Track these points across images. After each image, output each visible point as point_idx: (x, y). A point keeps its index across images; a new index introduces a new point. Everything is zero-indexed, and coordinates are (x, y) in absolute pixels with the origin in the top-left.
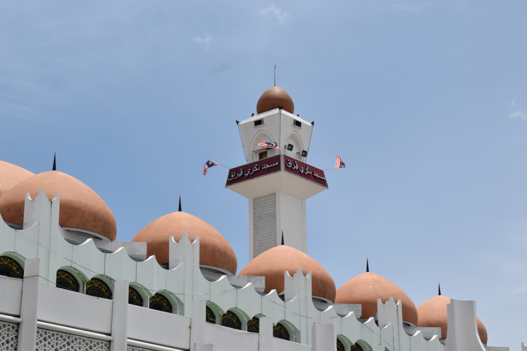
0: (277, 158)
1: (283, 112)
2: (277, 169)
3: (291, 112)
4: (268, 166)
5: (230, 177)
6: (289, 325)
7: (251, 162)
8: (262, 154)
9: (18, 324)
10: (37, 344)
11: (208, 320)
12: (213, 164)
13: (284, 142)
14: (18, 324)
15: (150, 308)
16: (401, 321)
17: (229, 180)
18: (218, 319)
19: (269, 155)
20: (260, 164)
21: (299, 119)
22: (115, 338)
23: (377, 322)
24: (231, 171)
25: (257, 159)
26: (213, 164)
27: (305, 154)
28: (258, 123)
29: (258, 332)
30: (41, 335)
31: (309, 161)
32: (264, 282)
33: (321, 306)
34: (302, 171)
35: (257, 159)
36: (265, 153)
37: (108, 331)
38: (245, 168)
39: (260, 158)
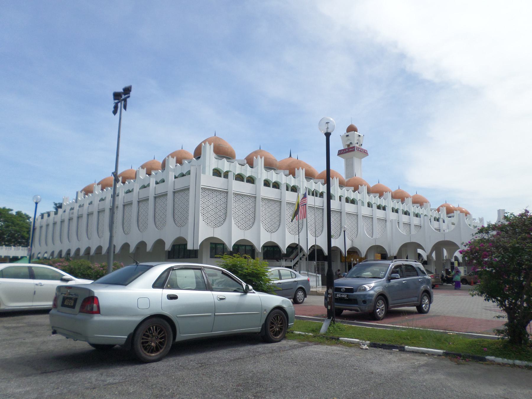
0: (354, 147)
1: (355, 132)
2: (354, 150)
3: (357, 132)
4: (351, 149)
5: (338, 152)
6: (221, 170)
7: (345, 148)
8: (348, 145)
9: (323, 209)
10: (201, 193)
11: (368, 207)
12: (127, 91)
13: (356, 142)
14: (227, 192)
15: (246, 182)
16: (367, 192)
17: (129, 95)
18: (290, 189)
19: (351, 146)
20: (348, 149)
21: (360, 135)
22: (229, 191)
23: (359, 192)
24: (339, 151)
25: (347, 147)
26: (127, 91)
27: (361, 145)
28: (347, 136)
29: (274, 187)
30: (234, 195)
31: (363, 147)
32: (324, 181)
33: (342, 188)
34: (361, 151)
35: (347, 147)
36: (350, 145)
37: (340, 209)
38: (343, 150)
39: (348, 147)
